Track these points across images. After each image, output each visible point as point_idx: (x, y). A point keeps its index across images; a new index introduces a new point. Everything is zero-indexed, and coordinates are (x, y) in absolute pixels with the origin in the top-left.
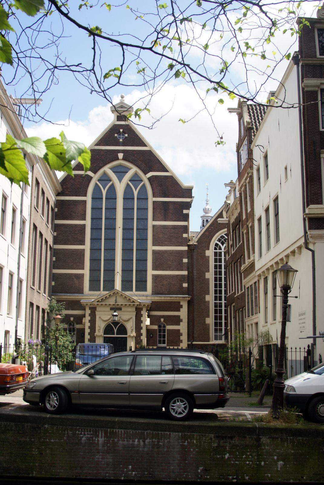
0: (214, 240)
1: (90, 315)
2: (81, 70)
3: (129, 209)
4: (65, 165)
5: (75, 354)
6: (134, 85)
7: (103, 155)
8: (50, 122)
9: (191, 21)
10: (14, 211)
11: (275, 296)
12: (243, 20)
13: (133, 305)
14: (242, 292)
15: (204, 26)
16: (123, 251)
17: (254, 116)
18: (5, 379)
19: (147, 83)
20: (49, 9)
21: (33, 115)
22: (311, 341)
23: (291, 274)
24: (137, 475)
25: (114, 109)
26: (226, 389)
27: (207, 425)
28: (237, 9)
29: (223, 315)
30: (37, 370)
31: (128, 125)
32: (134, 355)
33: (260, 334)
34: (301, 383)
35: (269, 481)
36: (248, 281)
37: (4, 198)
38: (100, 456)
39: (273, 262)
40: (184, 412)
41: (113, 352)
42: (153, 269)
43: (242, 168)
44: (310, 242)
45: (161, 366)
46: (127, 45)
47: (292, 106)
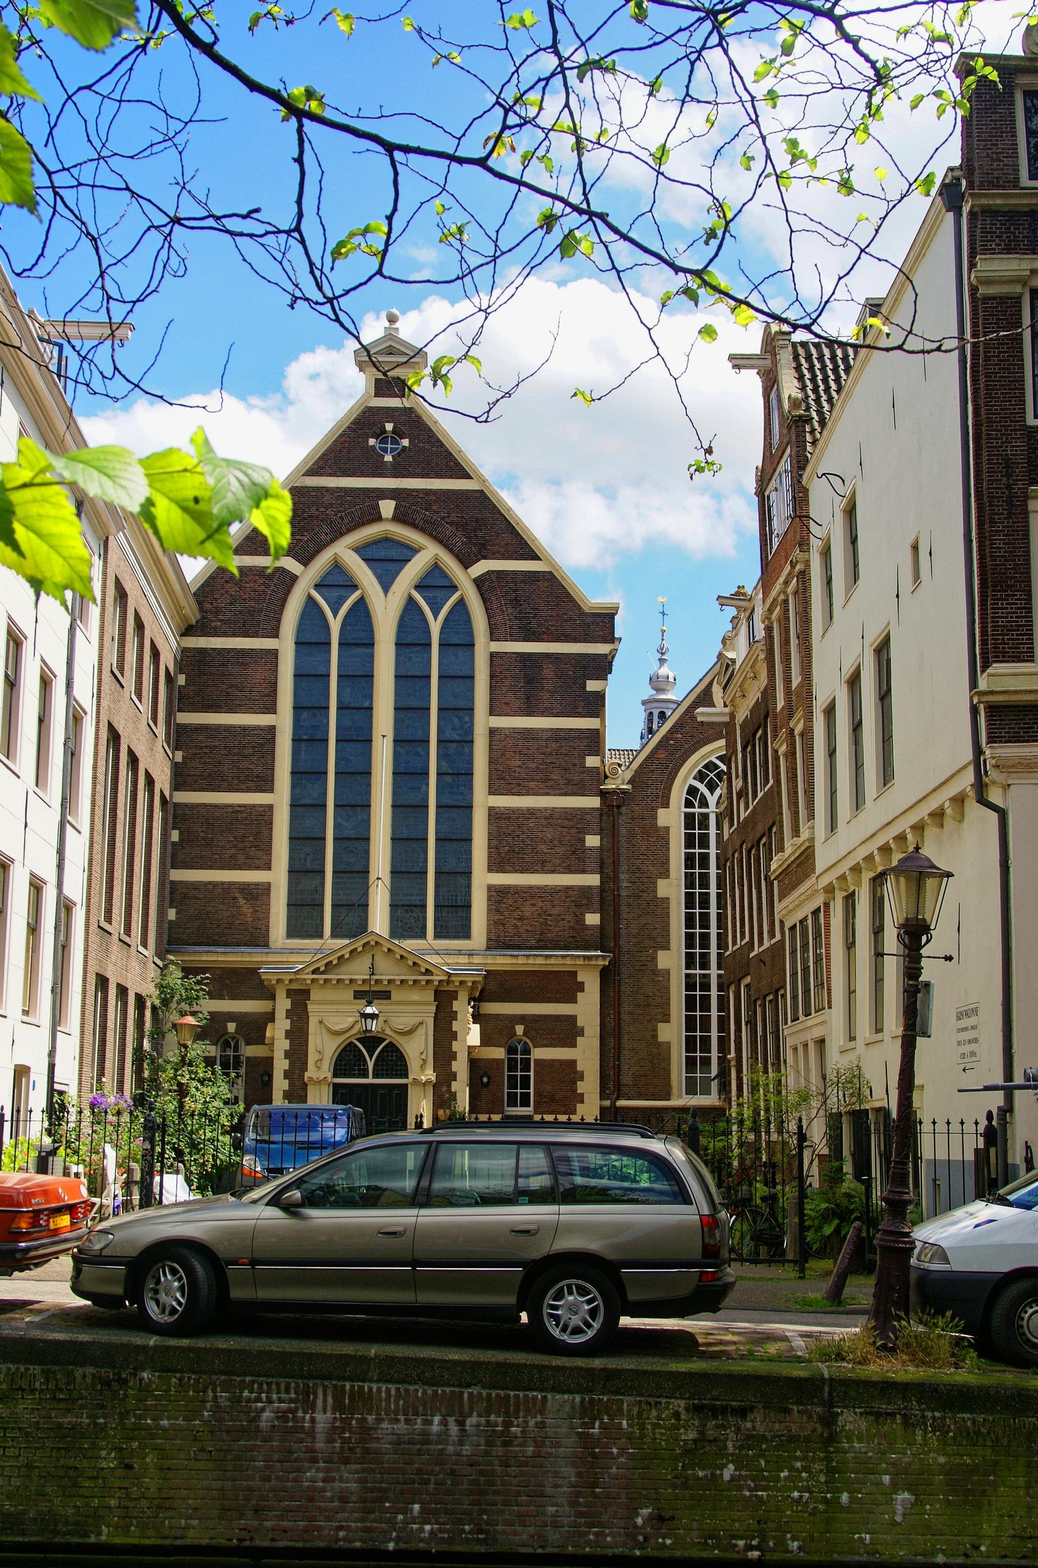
0: (685, 777)
1: (289, 1014)
2: (260, 229)
3: (413, 677)
4: (209, 537)
5: (242, 1140)
6: (429, 281)
7: (331, 505)
8: (161, 397)
9: (612, 70)
10: (46, 683)
11: (879, 954)
12: (782, 66)
13: (428, 982)
14: (774, 941)
15: (653, 88)
16: (393, 812)
17: (813, 379)
18: (12, 1222)
19: (470, 272)
20: (151, 29)
21: (104, 377)
22: (997, 1100)
23: (930, 883)
24: (439, 1535)
25: (367, 359)
26: (725, 1254)
27: (665, 1369)
28: (761, 30)
29: (714, 1013)
30: (119, 1192)
31: (411, 410)
32: (430, 1143)
33: (831, 1076)
34: (965, 1233)
35: (865, 1558)
36: (794, 908)
37: (11, 643)
38: (318, 1470)
39: (873, 847)
40: (589, 1326)
41: (364, 1132)
42: (490, 870)
43: (775, 547)
44: (994, 783)
45: (517, 1176)
46: (407, 150)
47: (938, 344)
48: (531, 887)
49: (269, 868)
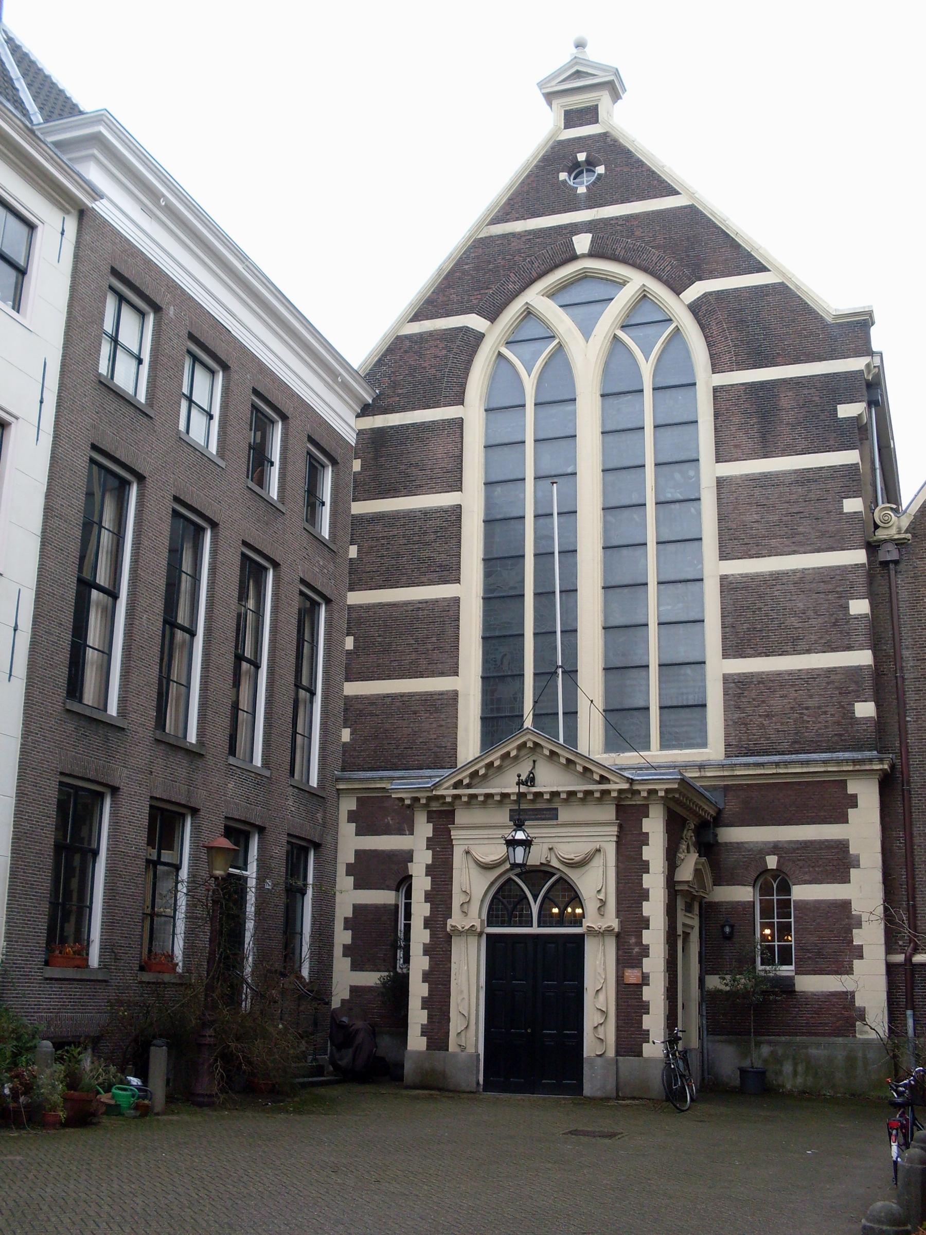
31: (605, 135)
42: (726, 655)
48: (779, 674)
49: (456, 674)
